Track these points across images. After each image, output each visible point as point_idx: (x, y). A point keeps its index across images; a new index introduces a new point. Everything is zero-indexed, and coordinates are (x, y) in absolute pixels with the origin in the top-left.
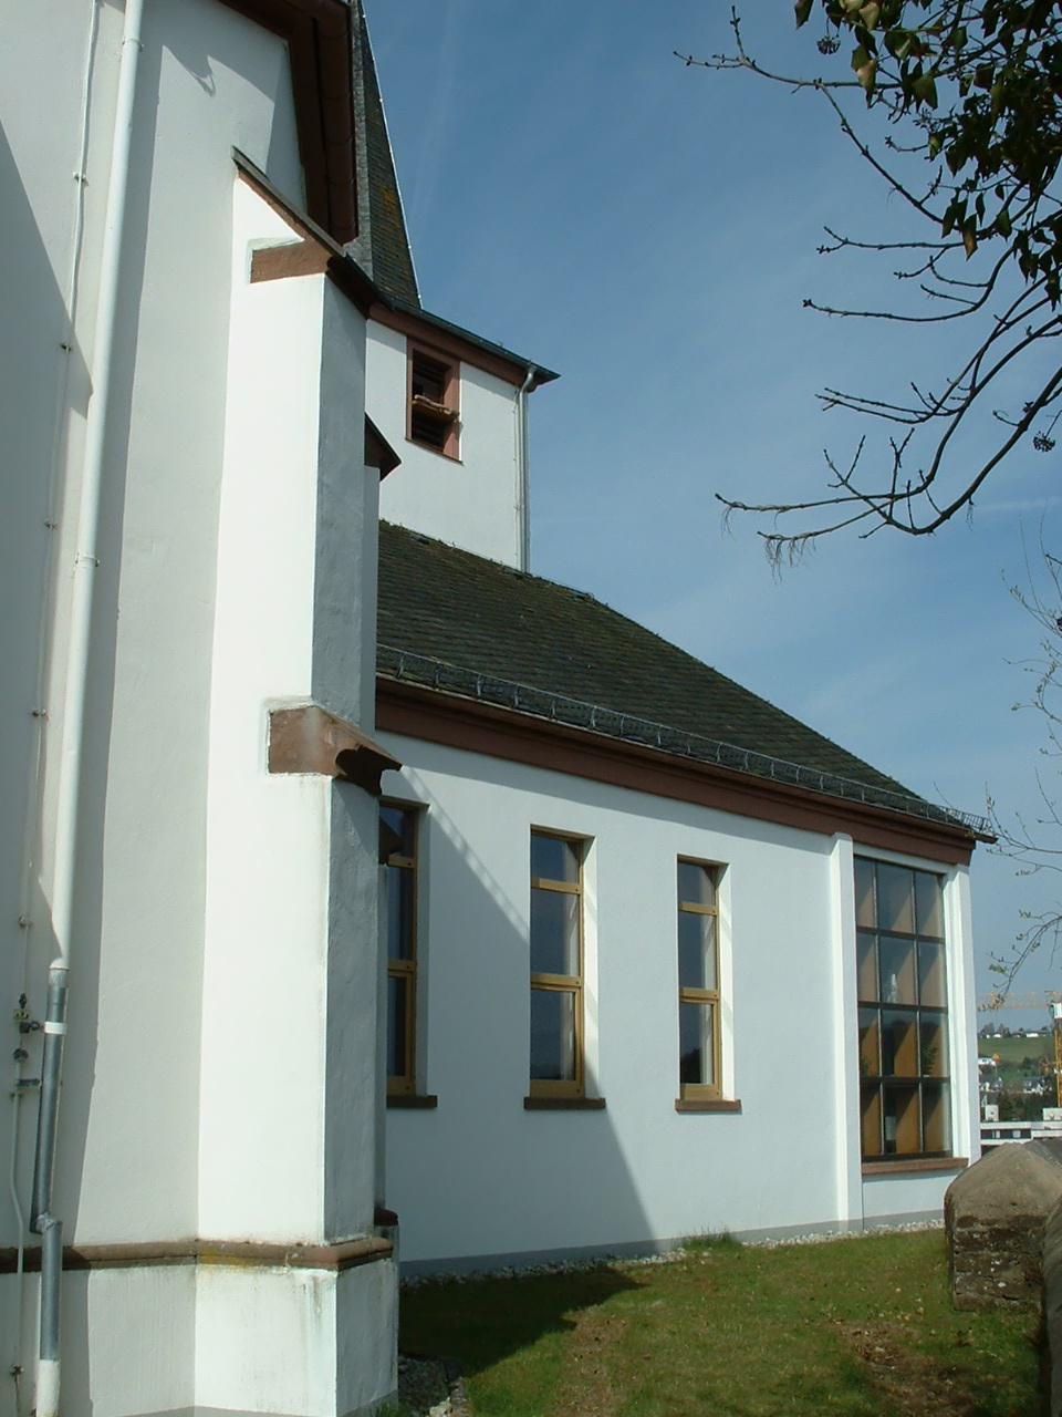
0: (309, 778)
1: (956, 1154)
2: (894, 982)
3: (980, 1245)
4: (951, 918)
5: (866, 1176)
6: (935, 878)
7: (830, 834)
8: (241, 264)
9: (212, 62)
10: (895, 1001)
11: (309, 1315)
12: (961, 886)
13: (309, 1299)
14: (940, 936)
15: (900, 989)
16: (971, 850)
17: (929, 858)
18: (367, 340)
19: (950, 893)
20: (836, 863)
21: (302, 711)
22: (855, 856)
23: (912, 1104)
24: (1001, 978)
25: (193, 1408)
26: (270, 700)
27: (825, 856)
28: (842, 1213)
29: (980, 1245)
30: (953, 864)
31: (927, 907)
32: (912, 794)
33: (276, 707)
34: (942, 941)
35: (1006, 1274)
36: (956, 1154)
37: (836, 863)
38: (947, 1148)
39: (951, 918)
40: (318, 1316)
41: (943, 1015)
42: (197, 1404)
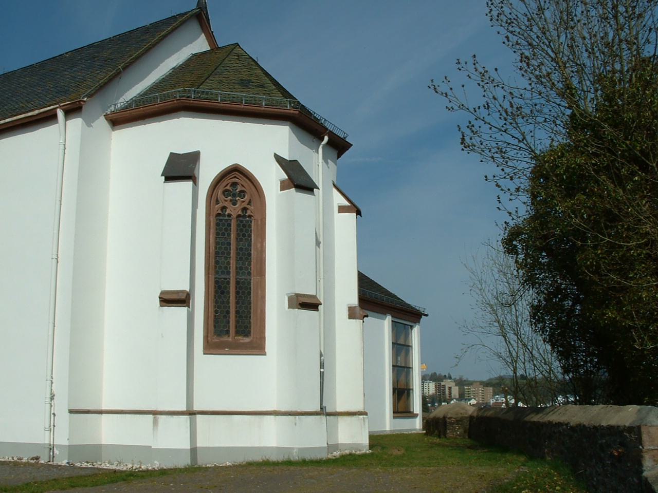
0: (358, 320)
1: (415, 413)
2: (399, 359)
3: (453, 424)
4: (415, 338)
5: (394, 417)
6: (409, 327)
7: (385, 314)
8: (336, 209)
9: (329, 161)
10: (399, 365)
11: (363, 423)
12: (418, 329)
13: (362, 421)
14: (410, 345)
15: (401, 362)
16: (420, 319)
17: (405, 320)
18: (287, 177)
19: (414, 333)
20: (386, 323)
21: (355, 307)
22: (392, 321)
23: (403, 397)
24: (457, 360)
25: (338, 444)
26: (348, 305)
27: (383, 321)
28: (388, 428)
29: (453, 424)
30: (415, 323)
31: (407, 336)
32: (401, 300)
33: (349, 306)
34: (412, 347)
35: (460, 430)
36: (415, 413)
37: (386, 323)
38: (412, 410)
39: (415, 338)
40: (364, 424)
41: (411, 369)
42: (339, 443)
